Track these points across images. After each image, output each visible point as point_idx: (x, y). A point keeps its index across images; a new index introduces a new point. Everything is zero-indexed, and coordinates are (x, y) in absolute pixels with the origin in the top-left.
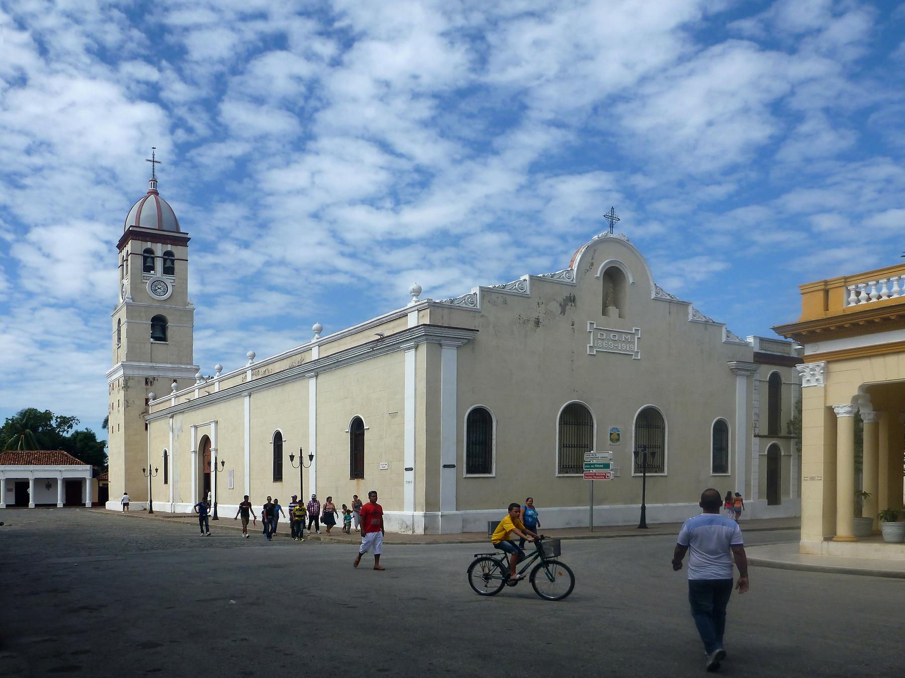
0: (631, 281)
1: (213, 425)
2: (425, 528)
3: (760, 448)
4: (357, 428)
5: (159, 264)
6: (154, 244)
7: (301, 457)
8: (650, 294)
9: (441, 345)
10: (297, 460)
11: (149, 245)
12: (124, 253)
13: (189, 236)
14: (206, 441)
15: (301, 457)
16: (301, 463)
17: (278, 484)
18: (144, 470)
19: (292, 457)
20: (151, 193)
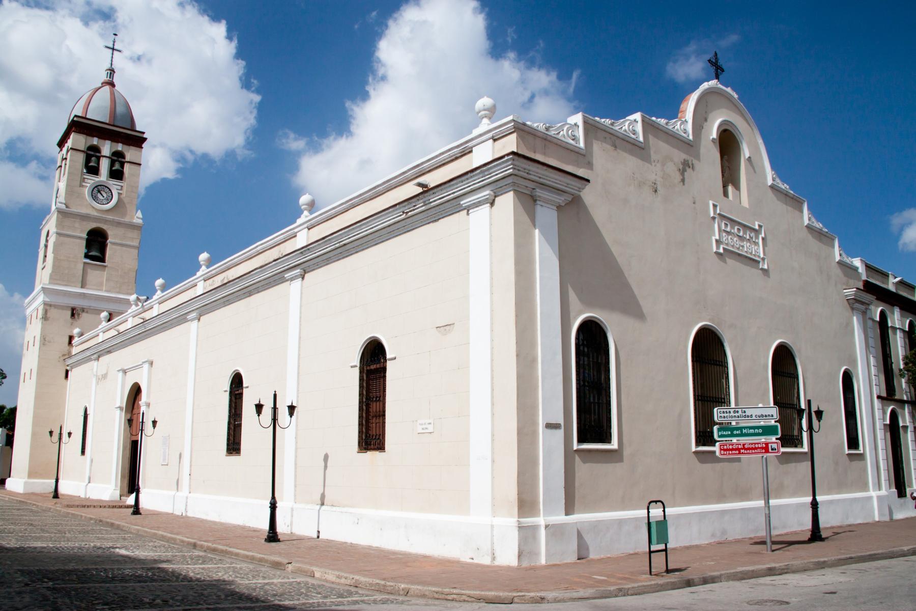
0: (747, 155)
1: (146, 366)
2: (520, 555)
3: (882, 417)
4: (374, 356)
5: (104, 165)
6: (101, 141)
7: (275, 408)
8: (766, 178)
9: (534, 199)
10: (267, 411)
11: (95, 141)
12: (65, 149)
13: (145, 136)
14: (136, 391)
15: (275, 408)
16: (274, 420)
17: (234, 458)
18: (51, 433)
19: (259, 408)
20: (105, 83)
